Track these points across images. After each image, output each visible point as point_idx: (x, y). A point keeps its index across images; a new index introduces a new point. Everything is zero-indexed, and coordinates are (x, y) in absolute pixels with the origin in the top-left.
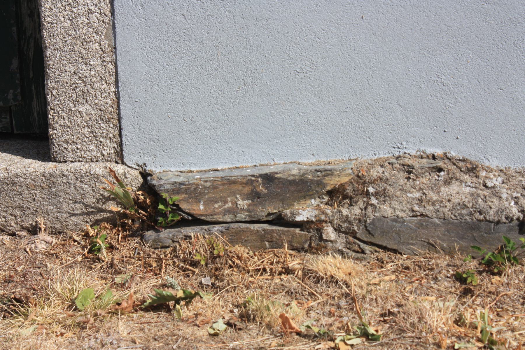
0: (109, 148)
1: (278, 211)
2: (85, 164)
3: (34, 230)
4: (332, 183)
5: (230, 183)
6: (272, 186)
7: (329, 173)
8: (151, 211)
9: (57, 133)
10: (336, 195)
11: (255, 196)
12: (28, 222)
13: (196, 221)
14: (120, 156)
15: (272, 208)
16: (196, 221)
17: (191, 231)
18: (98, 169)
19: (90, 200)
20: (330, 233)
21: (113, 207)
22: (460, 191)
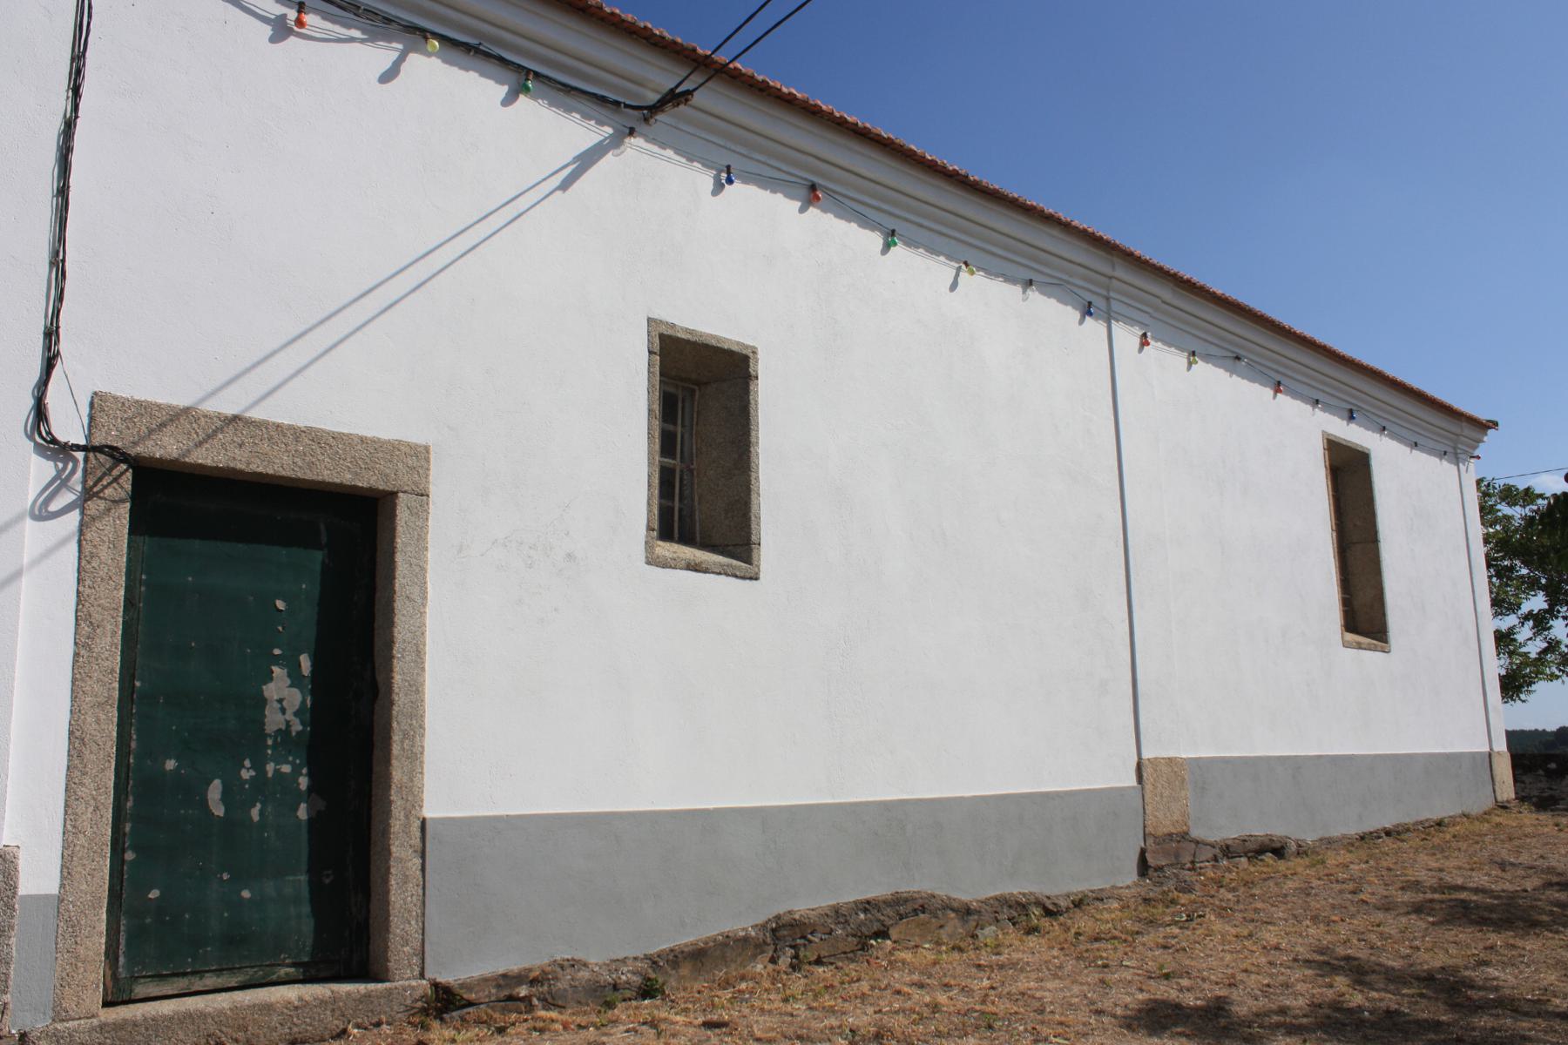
0: (417, 972)
1: (518, 995)
2: (407, 983)
3: (378, 1024)
4: (532, 975)
5: (485, 980)
6: (507, 980)
7: (530, 970)
8: (445, 1002)
9: (389, 488)
10: (534, 982)
11: (499, 986)
12: (375, 1020)
13: (470, 1004)
14: (422, 976)
15: (506, 993)
16: (470, 1004)
17: (470, 1010)
18: (414, 983)
19: (409, 1002)
20: (535, 1001)
21: (419, 1004)
22: (584, 974)
